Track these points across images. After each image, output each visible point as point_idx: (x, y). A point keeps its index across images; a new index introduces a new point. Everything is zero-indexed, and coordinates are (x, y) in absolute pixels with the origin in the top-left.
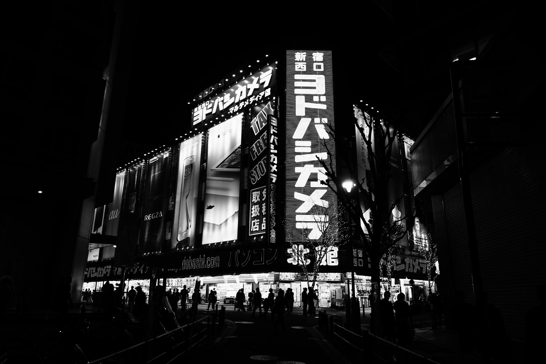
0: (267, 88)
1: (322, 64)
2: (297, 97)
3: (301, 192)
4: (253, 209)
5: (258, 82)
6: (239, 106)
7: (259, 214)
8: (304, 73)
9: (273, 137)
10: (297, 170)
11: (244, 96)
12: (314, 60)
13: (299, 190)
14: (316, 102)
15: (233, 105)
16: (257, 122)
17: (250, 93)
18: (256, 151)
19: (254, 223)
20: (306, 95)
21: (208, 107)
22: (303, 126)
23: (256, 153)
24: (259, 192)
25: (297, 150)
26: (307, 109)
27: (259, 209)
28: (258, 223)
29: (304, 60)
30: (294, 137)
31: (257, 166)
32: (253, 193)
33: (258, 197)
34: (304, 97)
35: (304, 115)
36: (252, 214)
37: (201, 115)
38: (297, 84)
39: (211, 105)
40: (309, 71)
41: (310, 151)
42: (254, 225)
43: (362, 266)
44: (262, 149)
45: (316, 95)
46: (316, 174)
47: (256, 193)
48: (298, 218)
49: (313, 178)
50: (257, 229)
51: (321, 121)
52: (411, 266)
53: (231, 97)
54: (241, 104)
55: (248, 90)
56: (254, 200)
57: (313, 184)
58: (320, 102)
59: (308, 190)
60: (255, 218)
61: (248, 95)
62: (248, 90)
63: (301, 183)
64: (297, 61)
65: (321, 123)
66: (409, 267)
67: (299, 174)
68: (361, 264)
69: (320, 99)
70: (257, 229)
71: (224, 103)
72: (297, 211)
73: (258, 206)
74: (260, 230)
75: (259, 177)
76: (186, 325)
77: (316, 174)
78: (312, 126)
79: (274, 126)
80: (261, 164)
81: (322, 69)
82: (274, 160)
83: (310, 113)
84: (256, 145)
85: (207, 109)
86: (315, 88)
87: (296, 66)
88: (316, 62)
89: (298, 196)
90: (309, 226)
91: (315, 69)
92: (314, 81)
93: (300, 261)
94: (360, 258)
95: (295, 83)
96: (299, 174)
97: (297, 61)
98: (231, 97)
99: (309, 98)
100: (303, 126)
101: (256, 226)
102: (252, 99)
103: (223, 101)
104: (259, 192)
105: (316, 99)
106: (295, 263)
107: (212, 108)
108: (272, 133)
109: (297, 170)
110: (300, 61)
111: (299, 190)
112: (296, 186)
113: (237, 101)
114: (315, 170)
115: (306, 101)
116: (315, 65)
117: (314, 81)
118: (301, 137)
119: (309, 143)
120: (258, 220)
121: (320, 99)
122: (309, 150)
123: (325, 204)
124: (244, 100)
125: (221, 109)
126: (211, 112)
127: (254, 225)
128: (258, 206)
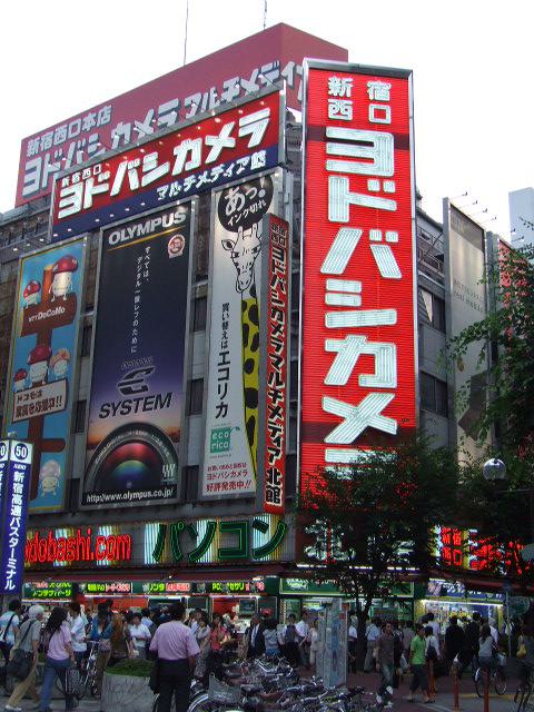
1: (388, 109)
10: (331, 345)
12: (371, 97)
21: (100, 180)
25: (331, 300)
29: (349, 95)
35: (347, 220)
40: (360, 122)
41: (359, 304)
49: (366, 363)
57: (366, 380)
59: (353, 393)
63: (338, 375)
64: (332, 96)
65: (384, 242)
78: (364, 246)
81: (388, 120)
86: (371, 161)
88: (374, 101)
89: (331, 405)
91: (372, 118)
92: (370, 144)
96: (334, 355)
99: (358, 183)
105: (373, 185)
109: (331, 345)
110: (338, 97)
114: (371, 348)
115: (352, 189)
117: (370, 144)
119: (355, 286)
122: (357, 301)
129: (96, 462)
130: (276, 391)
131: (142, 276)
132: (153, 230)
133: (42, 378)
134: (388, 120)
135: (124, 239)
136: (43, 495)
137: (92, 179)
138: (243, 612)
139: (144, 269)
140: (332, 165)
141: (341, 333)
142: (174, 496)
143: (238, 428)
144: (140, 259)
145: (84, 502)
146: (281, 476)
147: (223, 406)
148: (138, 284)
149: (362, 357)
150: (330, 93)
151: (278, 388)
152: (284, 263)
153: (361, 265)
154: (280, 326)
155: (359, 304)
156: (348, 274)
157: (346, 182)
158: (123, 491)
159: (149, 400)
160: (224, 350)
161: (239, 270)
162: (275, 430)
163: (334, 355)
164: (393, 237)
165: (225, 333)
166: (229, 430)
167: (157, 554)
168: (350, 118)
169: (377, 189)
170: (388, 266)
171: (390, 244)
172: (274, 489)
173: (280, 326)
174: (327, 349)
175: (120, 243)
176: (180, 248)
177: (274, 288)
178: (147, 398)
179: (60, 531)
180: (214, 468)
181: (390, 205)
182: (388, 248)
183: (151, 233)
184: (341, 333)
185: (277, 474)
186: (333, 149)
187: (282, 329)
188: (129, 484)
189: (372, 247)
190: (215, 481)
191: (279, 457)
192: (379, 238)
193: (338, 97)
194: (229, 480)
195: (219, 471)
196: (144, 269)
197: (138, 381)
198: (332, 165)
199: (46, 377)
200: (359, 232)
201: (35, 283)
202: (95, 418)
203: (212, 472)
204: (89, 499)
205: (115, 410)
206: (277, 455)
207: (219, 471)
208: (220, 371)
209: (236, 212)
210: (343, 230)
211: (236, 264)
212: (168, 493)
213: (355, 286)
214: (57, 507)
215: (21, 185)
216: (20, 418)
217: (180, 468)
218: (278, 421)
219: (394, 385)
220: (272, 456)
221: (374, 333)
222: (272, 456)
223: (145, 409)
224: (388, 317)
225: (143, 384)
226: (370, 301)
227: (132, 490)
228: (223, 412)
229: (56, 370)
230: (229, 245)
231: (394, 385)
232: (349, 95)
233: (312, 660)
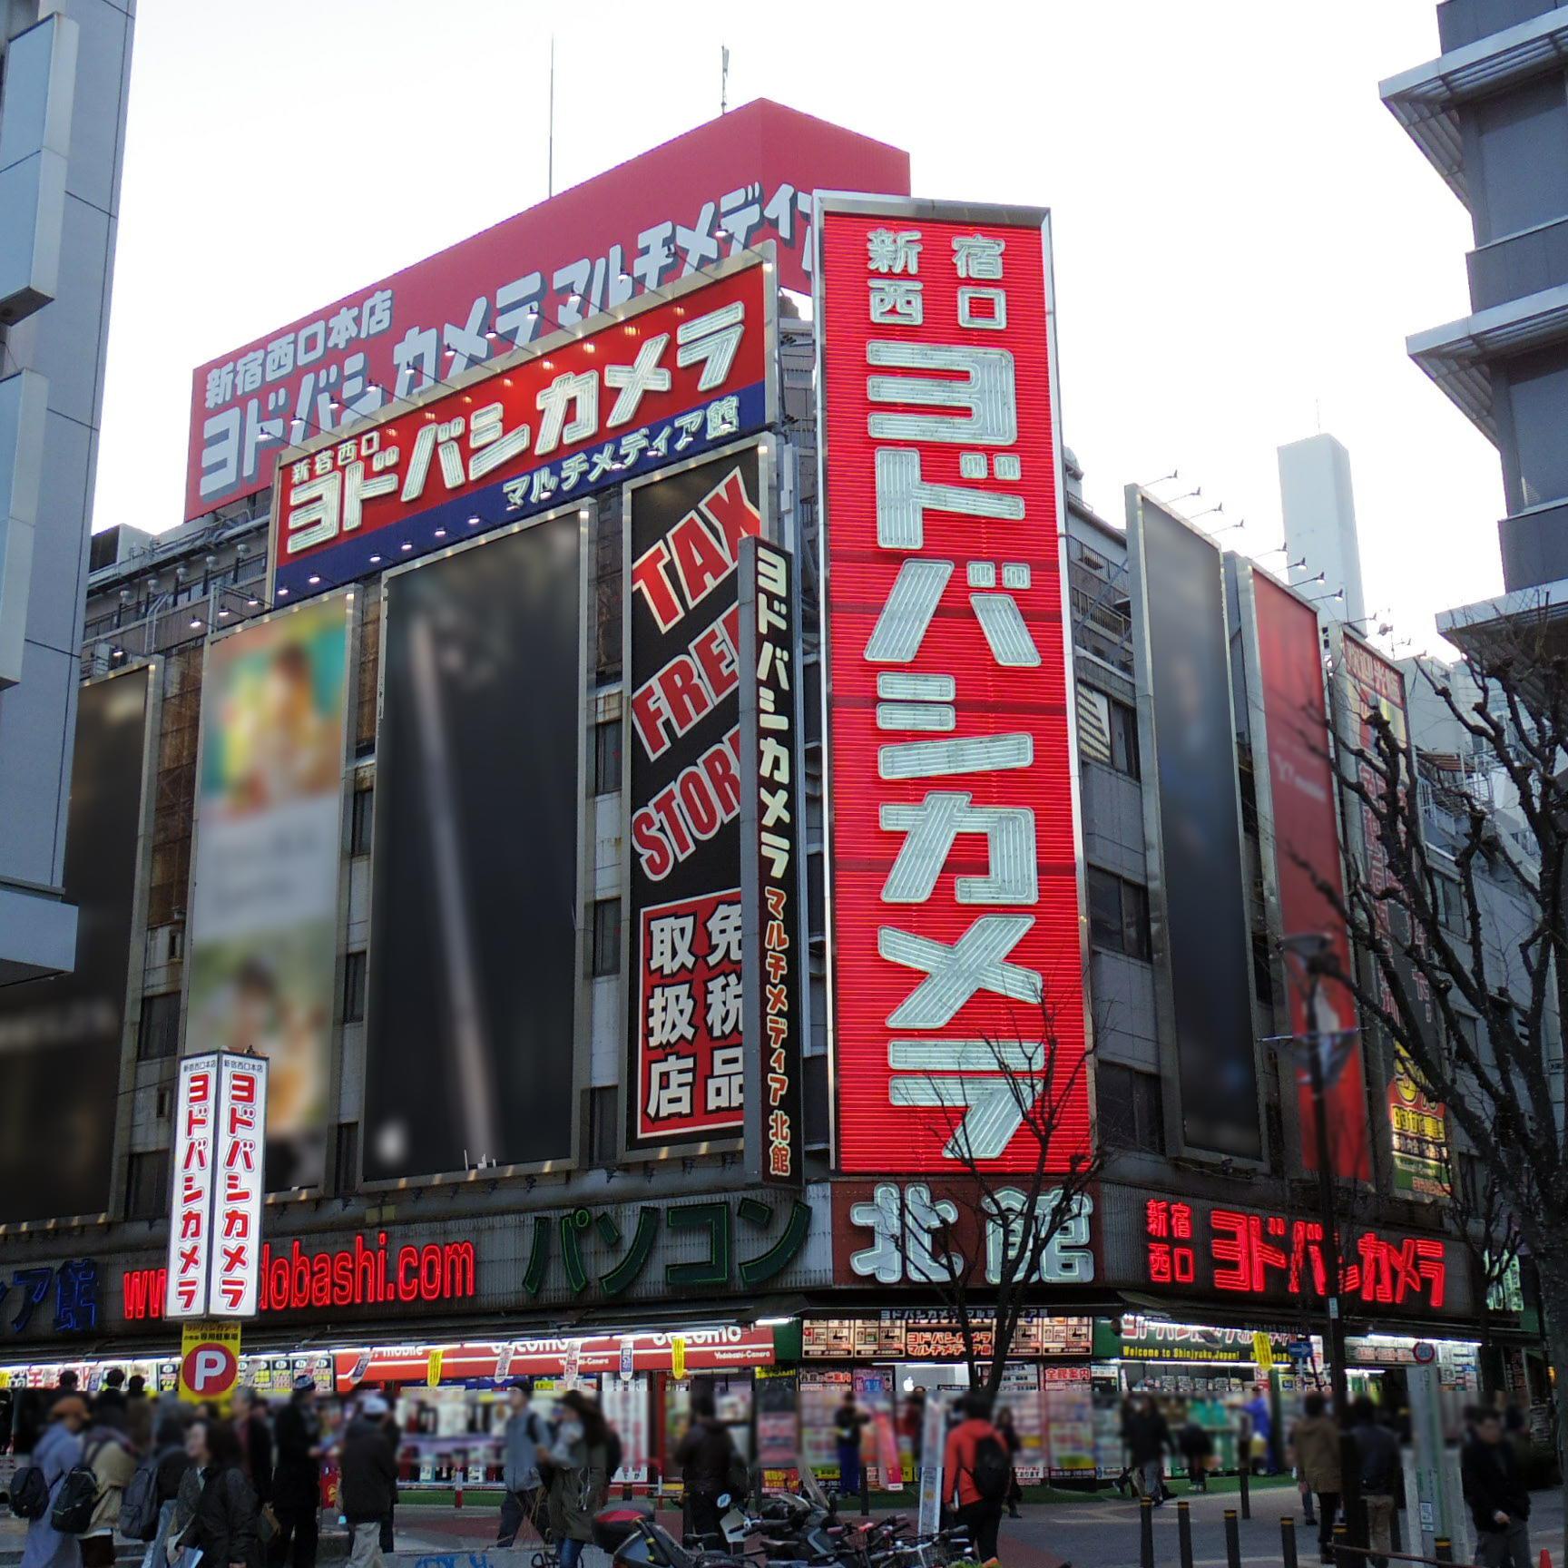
0: (717, 393)
1: (1000, 298)
2: (881, 456)
3: (908, 928)
4: (656, 1004)
5: (667, 360)
6: (556, 471)
7: (689, 1032)
9: (768, 648)
10: (893, 817)
11: (587, 423)
12: (962, 273)
13: (910, 918)
14: (973, 484)
15: (523, 463)
16: (670, 568)
17: (622, 412)
18: (667, 713)
19: (665, 1077)
20: (924, 448)
22: (916, 596)
23: (667, 724)
24: (688, 922)
25: (888, 719)
26: (930, 516)
27: (688, 1005)
28: (688, 1077)
29: (913, 269)
30: (872, 655)
31: (675, 787)
32: (655, 926)
33: (683, 946)
34: (915, 456)
36: (649, 1032)
37: (331, 498)
38: (883, 389)
39: (391, 457)
40: (938, 328)
41: (951, 726)
42: (664, 1085)
43: (1189, 1279)
44: (700, 704)
45: (973, 448)
47: (670, 922)
48: (901, 1055)
49: (970, 855)
50: (684, 1107)
51: (999, 578)
52: (1385, 1268)
53: (508, 425)
54: (573, 468)
55: (608, 397)
56: (662, 960)
57: (970, 890)
58: (991, 484)
59: (943, 918)
60: (666, 1050)
61: (611, 423)
62: (608, 397)
63: (911, 880)
64: (877, 274)
65: (999, 588)
66: (1378, 1280)
67: (899, 837)
68: (1184, 1271)
69: (990, 467)
70: (684, 1107)
71: (467, 454)
72: (894, 1022)
73: (683, 990)
74: (699, 1109)
75: (684, 847)
79: (772, 597)
80: (694, 778)
81: (1000, 321)
82: (776, 764)
83: (950, 536)
84: (666, 682)
85: (369, 474)
86: (965, 412)
87: (874, 299)
88: (969, 281)
89: (898, 947)
90: (954, 1094)
91: (964, 318)
92: (964, 376)
93: (911, 1268)
94: (1181, 1242)
96: (899, 837)
97: (877, 274)
98: (508, 425)
99: (940, 462)
100: (916, 596)
101: (673, 1091)
102: (633, 444)
103: (462, 440)
104: (688, 922)
105: (973, 467)
106: (891, 1277)
107: (400, 469)
108: (763, 629)
109: (893, 817)
110: (890, 275)
112: (889, 896)
113: (546, 444)
114: (977, 820)
115: (928, 476)
116: (964, 297)
117: (964, 376)
118: (908, 658)
119: (942, 687)
120: (689, 1063)
121: (990, 467)
123: (1022, 985)
124: (589, 446)
125: (452, 475)
126: (398, 492)
127: (664, 1085)
128: (683, 990)
134: (1000, 321)
140: (881, 426)
141: (913, 790)
150: (872, 266)
156: (920, 665)
164: (1018, 576)
168: (919, 321)
170: (1011, 643)
171: (1016, 594)
174: (886, 825)
181: (1011, 509)
182: (1009, 599)
184: (913, 790)
189: (975, 600)
193: (890, 275)
198: (881, 426)
210: (910, 569)
213: (942, 687)
219: (1033, 899)
224: (1014, 751)
231: (1033, 899)
232: (913, 269)
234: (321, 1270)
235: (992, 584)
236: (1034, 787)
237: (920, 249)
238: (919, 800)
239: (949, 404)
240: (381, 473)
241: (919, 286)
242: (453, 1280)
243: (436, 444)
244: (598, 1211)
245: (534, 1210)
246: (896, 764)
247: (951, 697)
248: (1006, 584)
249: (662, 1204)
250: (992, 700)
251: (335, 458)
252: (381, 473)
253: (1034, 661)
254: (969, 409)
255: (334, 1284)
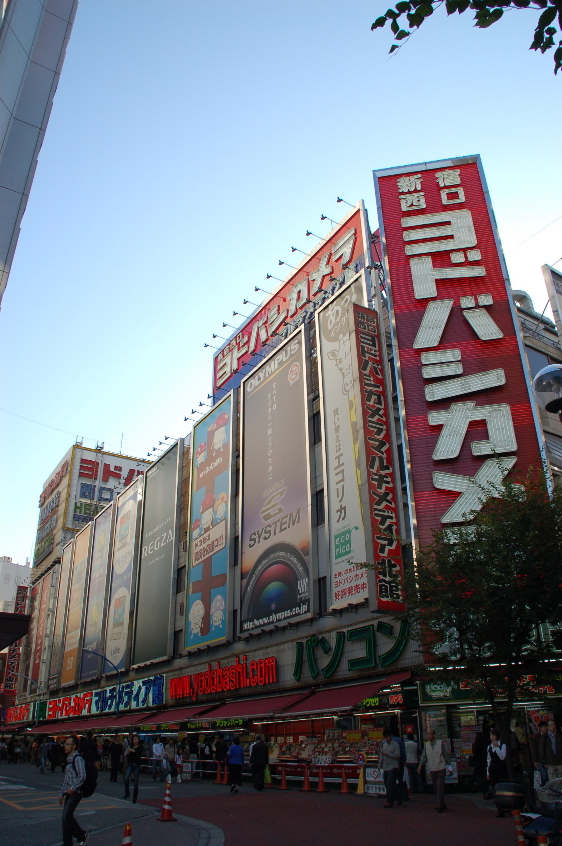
1: (461, 192)
2: (413, 262)
8: (421, 212)
10: (435, 418)
12: (442, 185)
13: (448, 465)
21: (241, 344)
22: (437, 317)
25: (428, 373)
29: (419, 188)
34: (429, 259)
35: (435, 294)
40: (434, 206)
46: (483, 423)
49: (478, 430)
57: (480, 448)
59: (466, 463)
63: (448, 447)
64: (403, 193)
65: (478, 306)
76: (490, 665)
77: (483, 423)
78: (456, 314)
81: (462, 198)
86: (451, 237)
88: (446, 187)
89: (444, 481)
91: (445, 201)
92: (448, 223)
95: (405, 234)
96: (439, 428)
99: (441, 259)
105: (457, 258)
109: (435, 418)
110: (409, 192)
111: (448, 465)
114: (479, 414)
117: (448, 223)
118: (436, 344)
119: (454, 354)
122: (459, 369)
126: (247, 352)
129: (249, 590)
130: (382, 477)
131: (272, 410)
132: (276, 367)
133: (210, 523)
134: (462, 198)
135: (257, 383)
136: (213, 629)
137: (237, 346)
138: (353, 728)
139: (273, 403)
140: (410, 250)
141: (444, 404)
142: (308, 611)
143: (356, 528)
144: (270, 395)
145: (242, 631)
146: (398, 568)
147: (342, 509)
148: (270, 417)
149: (473, 424)
150: (400, 191)
151: (383, 472)
152: (377, 349)
153: (457, 330)
154: (379, 409)
155: (461, 371)
156: (442, 346)
157: (429, 260)
158: (268, 615)
159: (284, 521)
160: (339, 453)
161: (343, 374)
162: (384, 518)
163: (439, 428)
164: (486, 300)
165: (338, 436)
166: (349, 532)
167: (298, 672)
168: (424, 206)
169: (463, 260)
170: (486, 328)
171: (487, 308)
172: (389, 582)
173: (379, 409)
174: (432, 423)
175: (255, 388)
176: (296, 374)
177: (367, 372)
178: (282, 519)
179: (464, 719)
180: (340, 574)
181: (478, 272)
182: (483, 311)
183: (276, 370)
184: (444, 404)
185: (391, 566)
186: (409, 236)
187: (381, 412)
188: (273, 606)
189: (466, 314)
190: (343, 587)
191: (393, 547)
192: (473, 304)
193: (409, 192)
194: (353, 584)
195: (344, 576)
196: (273, 403)
197: (274, 506)
198: (410, 250)
199: (212, 522)
200: (448, 304)
201: (203, 444)
202: (246, 548)
203: (338, 579)
204: (245, 626)
205: (259, 536)
206: (390, 544)
207: (344, 576)
208: (337, 474)
209: (336, 324)
210: (432, 305)
211: (341, 369)
212: (304, 608)
214: (223, 639)
215: (215, 380)
216: (197, 562)
217: (311, 582)
218: (387, 507)
219: (514, 447)
220: (383, 547)
221: (483, 397)
222: (383, 547)
223: (281, 530)
224: (495, 378)
225: (278, 507)
226: (471, 367)
227: (276, 612)
228: (342, 516)
229: (218, 514)
230: (334, 355)
231: (514, 447)
232: (419, 188)
233: (121, 760)
234: (226, 674)
235: (474, 305)
236: (511, 394)
237: (421, 180)
238: (448, 408)
239: (443, 235)
240: (243, 346)
241: (423, 194)
242: (273, 675)
243: (258, 328)
244: (320, 637)
245: (334, 630)
246: (435, 393)
247: (459, 358)
248: (481, 304)
249: (345, 630)
250: (480, 355)
251: (229, 348)
252: (243, 346)
253: (499, 335)
254: (453, 235)
255: (230, 680)
